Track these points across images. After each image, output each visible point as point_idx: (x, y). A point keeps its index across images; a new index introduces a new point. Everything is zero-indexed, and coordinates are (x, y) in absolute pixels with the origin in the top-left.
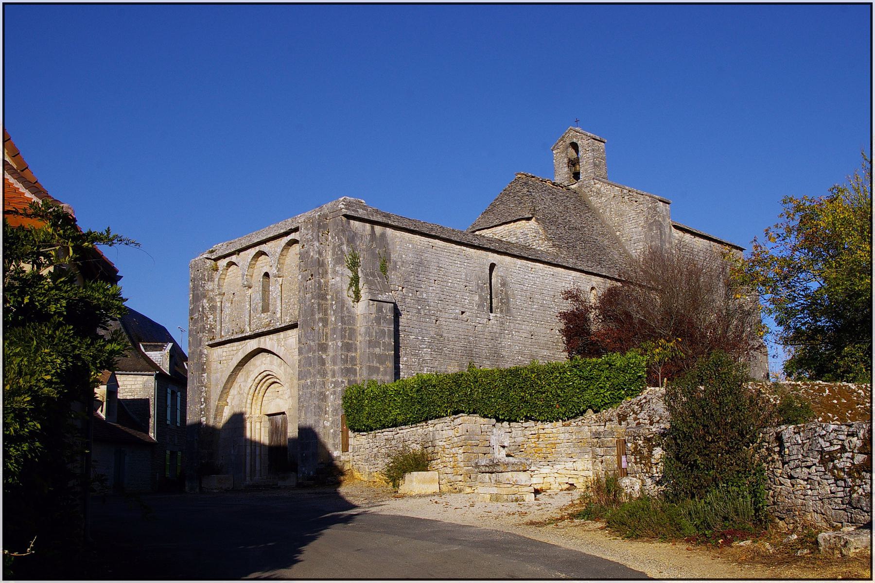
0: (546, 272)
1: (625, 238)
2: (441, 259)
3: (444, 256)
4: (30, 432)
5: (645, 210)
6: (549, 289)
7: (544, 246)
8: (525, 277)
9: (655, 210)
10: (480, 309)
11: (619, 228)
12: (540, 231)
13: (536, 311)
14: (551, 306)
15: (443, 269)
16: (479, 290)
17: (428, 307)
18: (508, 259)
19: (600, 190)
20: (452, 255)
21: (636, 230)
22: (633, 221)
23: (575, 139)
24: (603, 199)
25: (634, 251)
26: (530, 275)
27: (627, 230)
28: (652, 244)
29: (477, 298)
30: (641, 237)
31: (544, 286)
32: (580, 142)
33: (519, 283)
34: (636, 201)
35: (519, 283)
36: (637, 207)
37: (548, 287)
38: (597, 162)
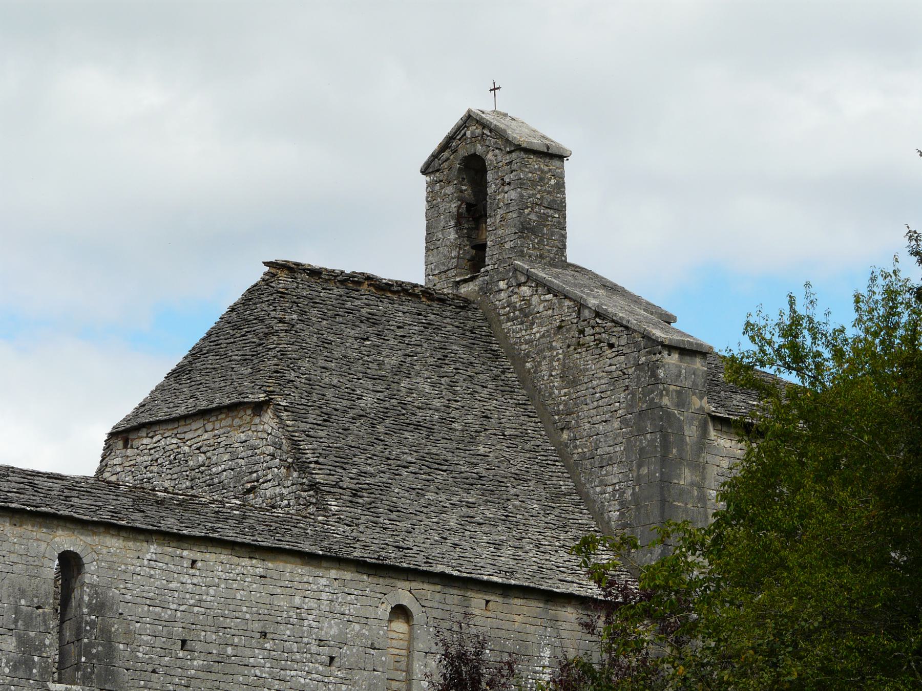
0: (239, 569)
1: (580, 450)
4: (609, 665)
5: (631, 371)
6: (248, 616)
7: (289, 483)
8: (171, 585)
9: (654, 375)
10: (21, 673)
11: (568, 419)
12: (284, 441)
13: (201, 674)
14: (252, 660)
16: (20, 623)
18: (113, 544)
19: (528, 303)
21: (608, 427)
22: (600, 403)
23: (479, 146)
24: (534, 331)
25: (598, 489)
26: (186, 579)
27: (587, 426)
30: (618, 449)
31: (231, 607)
34: (611, 346)
37: (244, 609)
38: (533, 217)
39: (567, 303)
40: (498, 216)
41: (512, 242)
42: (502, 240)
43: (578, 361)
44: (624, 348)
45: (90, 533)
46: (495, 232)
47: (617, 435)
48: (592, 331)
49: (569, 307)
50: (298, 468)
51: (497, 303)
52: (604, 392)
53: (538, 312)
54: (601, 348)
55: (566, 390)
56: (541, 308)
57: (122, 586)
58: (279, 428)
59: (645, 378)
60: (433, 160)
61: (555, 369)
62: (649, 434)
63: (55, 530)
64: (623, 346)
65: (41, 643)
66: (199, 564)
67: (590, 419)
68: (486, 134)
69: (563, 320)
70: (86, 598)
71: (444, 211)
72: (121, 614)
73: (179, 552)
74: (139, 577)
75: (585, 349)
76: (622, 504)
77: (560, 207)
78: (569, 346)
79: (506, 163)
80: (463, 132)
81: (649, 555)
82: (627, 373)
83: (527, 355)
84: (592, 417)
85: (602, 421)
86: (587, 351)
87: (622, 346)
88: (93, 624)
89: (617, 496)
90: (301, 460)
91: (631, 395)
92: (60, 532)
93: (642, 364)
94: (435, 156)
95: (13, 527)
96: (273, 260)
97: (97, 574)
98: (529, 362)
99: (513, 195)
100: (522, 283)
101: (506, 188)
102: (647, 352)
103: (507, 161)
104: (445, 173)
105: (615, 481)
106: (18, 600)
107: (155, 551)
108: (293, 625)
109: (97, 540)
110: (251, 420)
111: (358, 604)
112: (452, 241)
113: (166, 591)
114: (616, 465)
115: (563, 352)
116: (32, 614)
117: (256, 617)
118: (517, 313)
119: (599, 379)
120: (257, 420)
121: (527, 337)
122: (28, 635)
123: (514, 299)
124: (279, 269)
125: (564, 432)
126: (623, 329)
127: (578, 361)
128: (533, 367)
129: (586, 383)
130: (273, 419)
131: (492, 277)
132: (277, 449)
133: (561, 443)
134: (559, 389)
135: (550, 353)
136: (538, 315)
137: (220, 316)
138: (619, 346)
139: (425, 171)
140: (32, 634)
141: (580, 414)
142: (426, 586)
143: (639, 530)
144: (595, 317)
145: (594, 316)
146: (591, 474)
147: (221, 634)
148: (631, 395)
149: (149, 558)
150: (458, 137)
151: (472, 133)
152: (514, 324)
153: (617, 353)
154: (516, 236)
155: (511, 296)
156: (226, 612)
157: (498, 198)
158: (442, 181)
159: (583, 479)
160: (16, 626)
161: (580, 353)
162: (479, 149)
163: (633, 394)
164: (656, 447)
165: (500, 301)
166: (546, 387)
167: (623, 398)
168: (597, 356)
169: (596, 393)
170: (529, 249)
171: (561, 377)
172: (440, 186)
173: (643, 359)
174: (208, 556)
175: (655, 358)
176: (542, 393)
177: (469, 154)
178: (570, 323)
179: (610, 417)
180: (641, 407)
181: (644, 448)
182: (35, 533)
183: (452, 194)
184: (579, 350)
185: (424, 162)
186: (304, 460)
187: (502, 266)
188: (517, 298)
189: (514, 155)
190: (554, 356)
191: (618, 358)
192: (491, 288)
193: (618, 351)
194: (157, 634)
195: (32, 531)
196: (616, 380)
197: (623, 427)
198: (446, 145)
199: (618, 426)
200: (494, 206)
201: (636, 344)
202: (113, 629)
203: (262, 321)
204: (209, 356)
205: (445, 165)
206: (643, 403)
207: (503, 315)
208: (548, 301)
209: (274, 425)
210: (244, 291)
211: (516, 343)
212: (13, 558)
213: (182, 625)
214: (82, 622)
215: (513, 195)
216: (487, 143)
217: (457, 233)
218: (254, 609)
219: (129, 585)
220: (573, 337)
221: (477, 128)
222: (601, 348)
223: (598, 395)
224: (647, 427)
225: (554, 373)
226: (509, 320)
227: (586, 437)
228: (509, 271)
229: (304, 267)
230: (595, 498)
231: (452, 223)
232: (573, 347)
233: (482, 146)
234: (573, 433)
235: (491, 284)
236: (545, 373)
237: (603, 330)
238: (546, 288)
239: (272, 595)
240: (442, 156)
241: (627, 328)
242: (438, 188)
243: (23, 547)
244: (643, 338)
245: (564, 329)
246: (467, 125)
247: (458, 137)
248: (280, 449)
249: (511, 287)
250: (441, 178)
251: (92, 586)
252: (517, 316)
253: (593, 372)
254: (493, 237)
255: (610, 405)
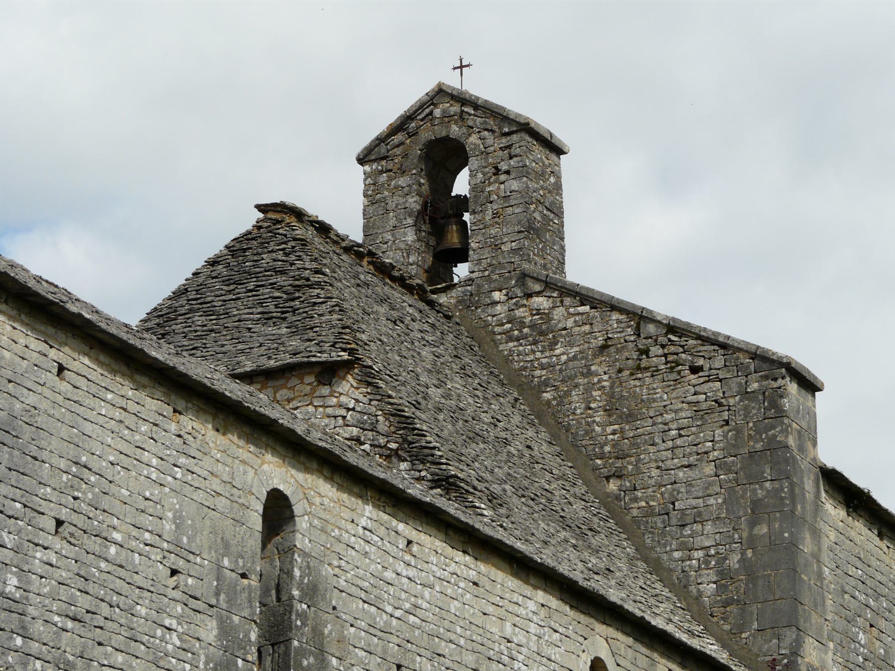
0: (453, 567)
1: (643, 504)
2: (88, 428)
3: (101, 420)
6: (462, 642)
12: (380, 418)
15: (93, 479)
16: (222, 597)
17: (19, 641)
19: (547, 316)
20: (130, 421)
24: (557, 352)
26: (400, 567)
27: (655, 473)
28: (756, 531)
29: (209, 631)
30: (712, 501)
32: (474, 139)
33: (363, 595)
34: (695, 370)
35: (363, 595)
36: (698, 389)
37: (459, 630)
38: (537, 216)
39: (615, 316)
40: (490, 212)
41: (513, 244)
42: (497, 241)
43: (638, 389)
44: (719, 372)
45: (302, 467)
46: (484, 231)
47: (710, 484)
48: (660, 352)
49: (619, 321)
50: (410, 456)
51: (489, 318)
52: (685, 428)
53: (565, 329)
54: (679, 372)
55: (616, 427)
56: (570, 323)
57: (335, 563)
58: (371, 400)
59: (759, 409)
60: (379, 145)
61: (595, 400)
62: (769, 482)
63: (264, 451)
64: (719, 369)
65: (246, 635)
66: (415, 548)
67: (660, 464)
68: (467, 113)
69: (609, 338)
70: (297, 573)
71: (396, 207)
72: (334, 608)
73: (394, 523)
74: (354, 553)
75: (649, 374)
76: (724, 576)
77: (557, 211)
78: (620, 371)
79: (501, 148)
80: (427, 111)
81: (775, 641)
82: (725, 403)
83: (546, 383)
84: (663, 461)
85: (682, 466)
86: (652, 376)
87: (716, 369)
88: (302, 616)
89: (713, 563)
90: (417, 445)
91: (734, 432)
92: (269, 457)
93: (753, 392)
94: (381, 140)
95: (216, 433)
96: (278, 202)
97: (308, 536)
98: (547, 392)
99: (515, 185)
100: (535, 293)
101: (503, 177)
102: (761, 376)
103: (502, 145)
104: (396, 161)
105: (707, 544)
106: (220, 557)
107: (370, 515)
108: (504, 665)
109: (309, 480)
110: (313, 391)
111: (563, 648)
112: (409, 243)
113: (381, 582)
114: (710, 523)
115: (610, 377)
116: (236, 585)
117: (470, 646)
118: (526, 330)
119: (676, 411)
120: (325, 390)
121: (544, 361)
122: (231, 619)
123: (520, 312)
124: (286, 213)
125: (611, 481)
126: (716, 348)
127: (638, 389)
128: (555, 399)
129: (651, 418)
130: (357, 388)
131: (479, 286)
132: (364, 430)
133: (608, 495)
134: (603, 426)
135: (586, 380)
136: (564, 332)
137: (193, 270)
138: (711, 369)
139: (362, 160)
140: (236, 619)
141: (642, 457)
142: (620, 636)
143: (755, 607)
144: (666, 334)
145: (665, 332)
146: (663, 534)
147: (436, 664)
148: (734, 432)
149: (364, 524)
150: (420, 117)
151: (444, 111)
152: (521, 345)
153: (707, 378)
154: (522, 235)
155: (513, 310)
156: (442, 630)
157: (488, 189)
158: (390, 171)
159: (648, 541)
160: (218, 600)
161: (640, 379)
162: (455, 130)
163: (738, 431)
164: (782, 499)
165: (493, 316)
166: (579, 423)
167: (719, 435)
168: (672, 383)
169: (669, 430)
170: (534, 254)
171: (605, 410)
172: (389, 177)
173: (755, 386)
174: (423, 538)
175: (775, 385)
176: (573, 431)
177: (438, 137)
178: (622, 341)
179: (697, 460)
180: (753, 447)
181: (760, 500)
182: (241, 450)
183: (409, 186)
184: (640, 376)
185: (363, 148)
186: (424, 444)
187: (497, 272)
188: (526, 312)
189: (515, 137)
190: (594, 384)
191: (711, 384)
192: (479, 300)
193: (709, 376)
194: (372, 649)
195: (239, 447)
196: (707, 413)
197: (721, 472)
198: (401, 125)
199: (712, 472)
200: (482, 199)
201: (739, 367)
202: (326, 632)
203: (283, 272)
204: (194, 316)
205: (398, 151)
206: (757, 442)
207: (500, 334)
208: (582, 314)
209: (361, 397)
210: (227, 241)
211: (525, 368)
212: (216, 485)
213: (397, 641)
214: (290, 612)
215: (515, 185)
216: (470, 123)
217: (416, 234)
218: (468, 632)
219: (343, 563)
220: (628, 359)
221: (451, 105)
222: (679, 372)
223: (674, 432)
224: (765, 472)
225: (593, 405)
226: (511, 339)
227: (654, 486)
228: (511, 278)
229: (311, 219)
230: (671, 567)
231: (410, 221)
232: (627, 373)
233: (460, 127)
234: (630, 481)
235: (478, 295)
236: (577, 405)
237: (681, 350)
238: (578, 298)
239: (485, 614)
240: (393, 140)
241: (724, 346)
242: (386, 178)
243: (227, 469)
244: (753, 359)
245: (612, 349)
246: (435, 102)
247: (420, 117)
248: (372, 430)
249: (512, 298)
250: (389, 167)
251: (305, 554)
252: (527, 334)
253: (665, 403)
254: (480, 238)
255: (695, 445)
